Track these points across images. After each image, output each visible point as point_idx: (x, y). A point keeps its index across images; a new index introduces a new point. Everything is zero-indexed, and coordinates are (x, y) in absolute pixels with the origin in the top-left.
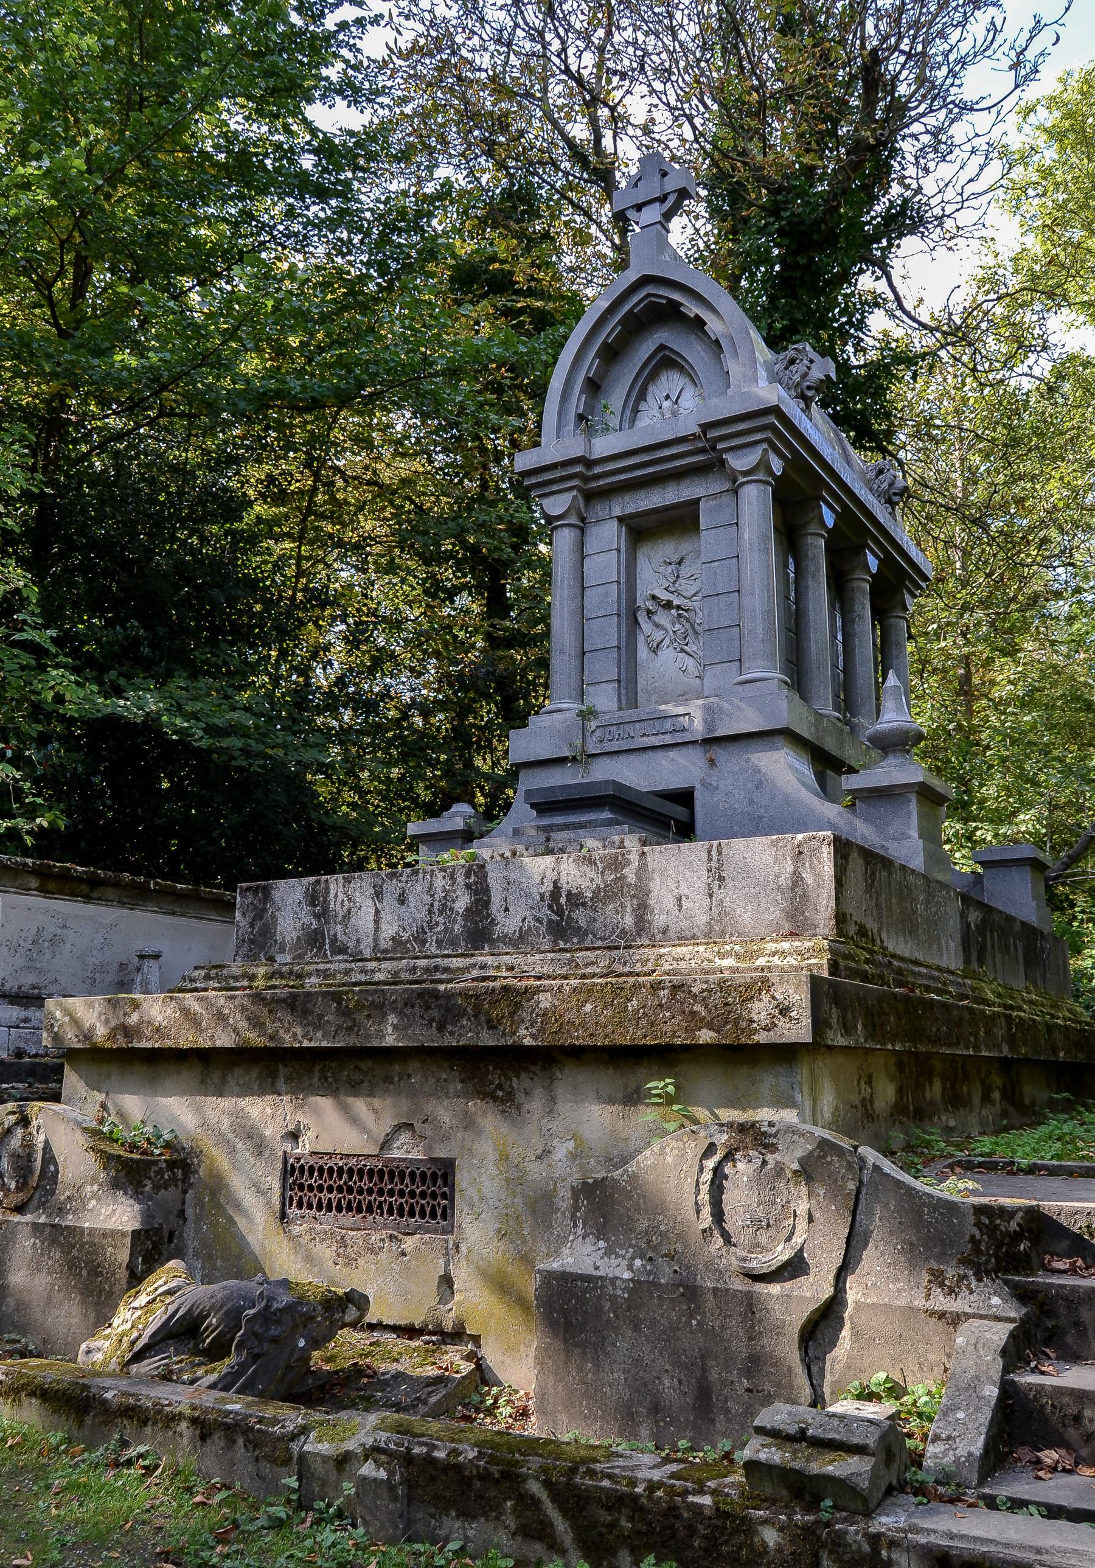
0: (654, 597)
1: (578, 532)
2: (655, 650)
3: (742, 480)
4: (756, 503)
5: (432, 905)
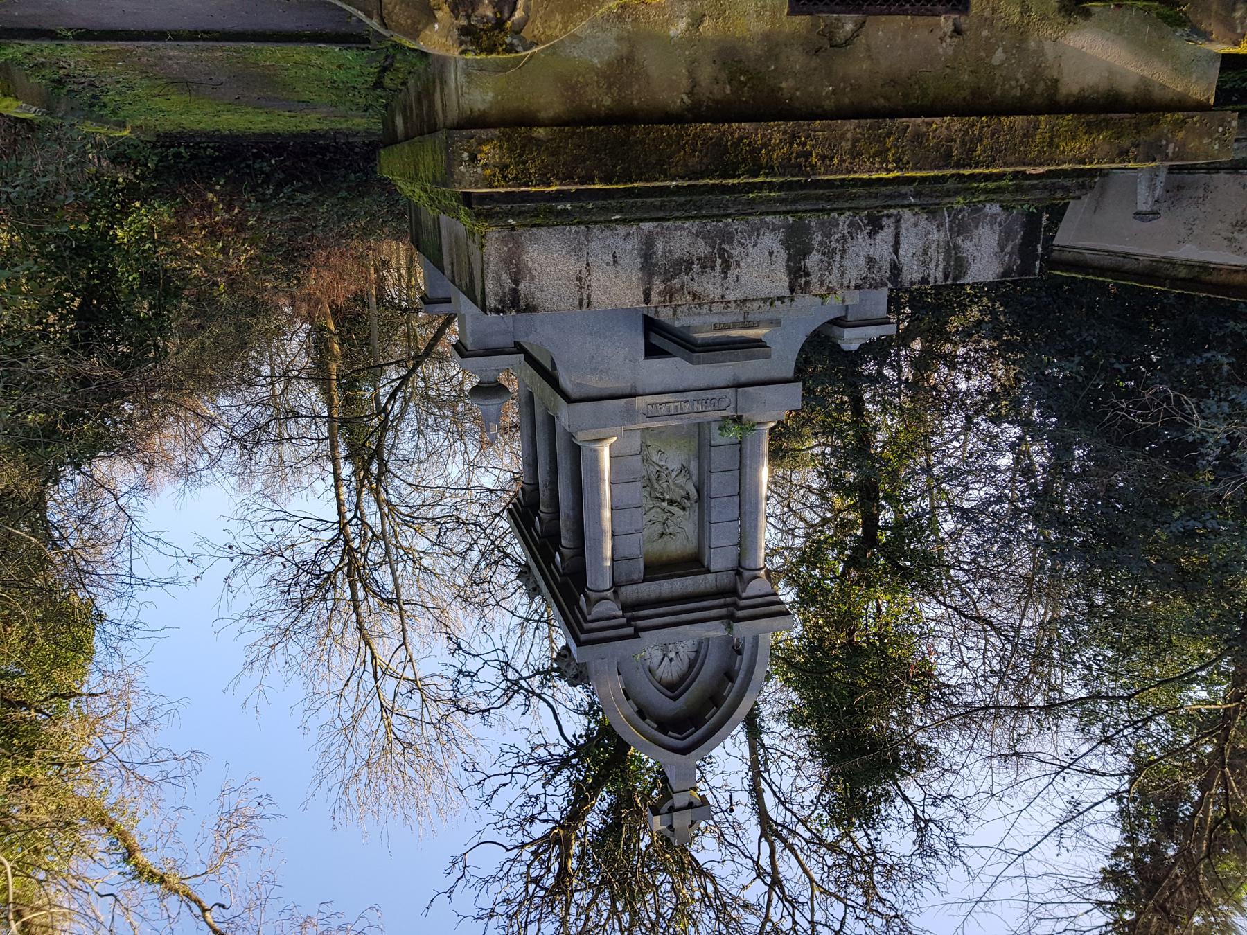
0: (684, 509)
3: (609, 594)
4: (600, 575)
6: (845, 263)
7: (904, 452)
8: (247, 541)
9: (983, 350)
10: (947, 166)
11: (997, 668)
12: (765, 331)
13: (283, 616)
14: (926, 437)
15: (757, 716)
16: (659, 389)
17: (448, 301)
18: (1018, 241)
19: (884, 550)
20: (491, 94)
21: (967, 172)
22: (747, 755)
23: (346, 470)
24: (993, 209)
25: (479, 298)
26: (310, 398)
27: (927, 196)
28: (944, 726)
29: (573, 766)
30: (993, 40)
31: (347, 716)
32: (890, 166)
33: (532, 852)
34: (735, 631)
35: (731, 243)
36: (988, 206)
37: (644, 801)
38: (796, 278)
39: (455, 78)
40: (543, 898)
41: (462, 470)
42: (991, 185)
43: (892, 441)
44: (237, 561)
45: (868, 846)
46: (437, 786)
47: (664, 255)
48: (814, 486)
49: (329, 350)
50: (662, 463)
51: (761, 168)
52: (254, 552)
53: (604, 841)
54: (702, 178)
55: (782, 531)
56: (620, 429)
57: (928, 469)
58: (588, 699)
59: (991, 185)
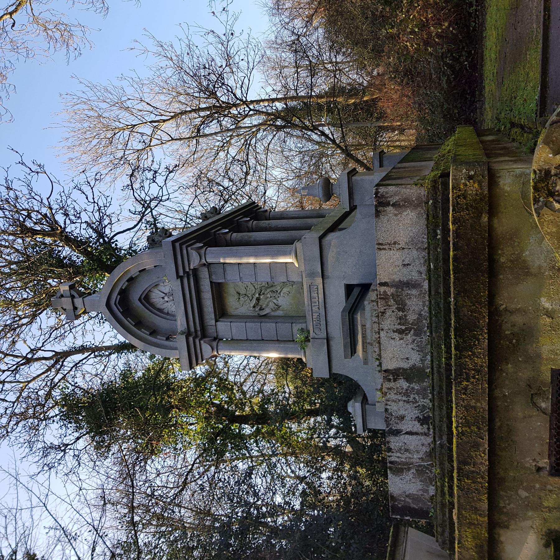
0: (254, 307)
1: (221, 341)
2: (278, 307)
5: (404, 401)
6: (401, 403)
7: (286, 440)
8: (236, 44)
9: (345, 488)
10: (459, 462)
11: (156, 493)
12: (361, 355)
13: (190, 66)
14: (293, 454)
15: (128, 351)
16: (327, 293)
17: (381, 166)
18: (412, 505)
19: (228, 426)
20: (509, 189)
21: (455, 475)
22: (104, 345)
23: (279, 106)
24: (432, 490)
25: (384, 183)
26: (322, 85)
27: (441, 451)
28: (123, 461)
29: (98, 240)
30: (533, 490)
31: (129, 104)
32: (460, 429)
33: (46, 214)
34: (180, 336)
35: (415, 335)
36: (434, 488)
37: (77, 282)
38: (392, 373)
39: (519, 168)
40: (19, 220)
41: (277, 176)
42: (446, 489)
43: (292, 433)
44: (224, 38)
45: (50, 416)
46: (86, 158)
47: (408, 295)
48: (265, 388)
49: (351, 97)
50: (282, 293)
51: (461, 352)
52: (229, 49)
53: (53, 258)
54: (455, 316)
55: (239, 368)
56: (303, 269)
57: (274, 454)
58: (139, 249)
59: (446, 489)
